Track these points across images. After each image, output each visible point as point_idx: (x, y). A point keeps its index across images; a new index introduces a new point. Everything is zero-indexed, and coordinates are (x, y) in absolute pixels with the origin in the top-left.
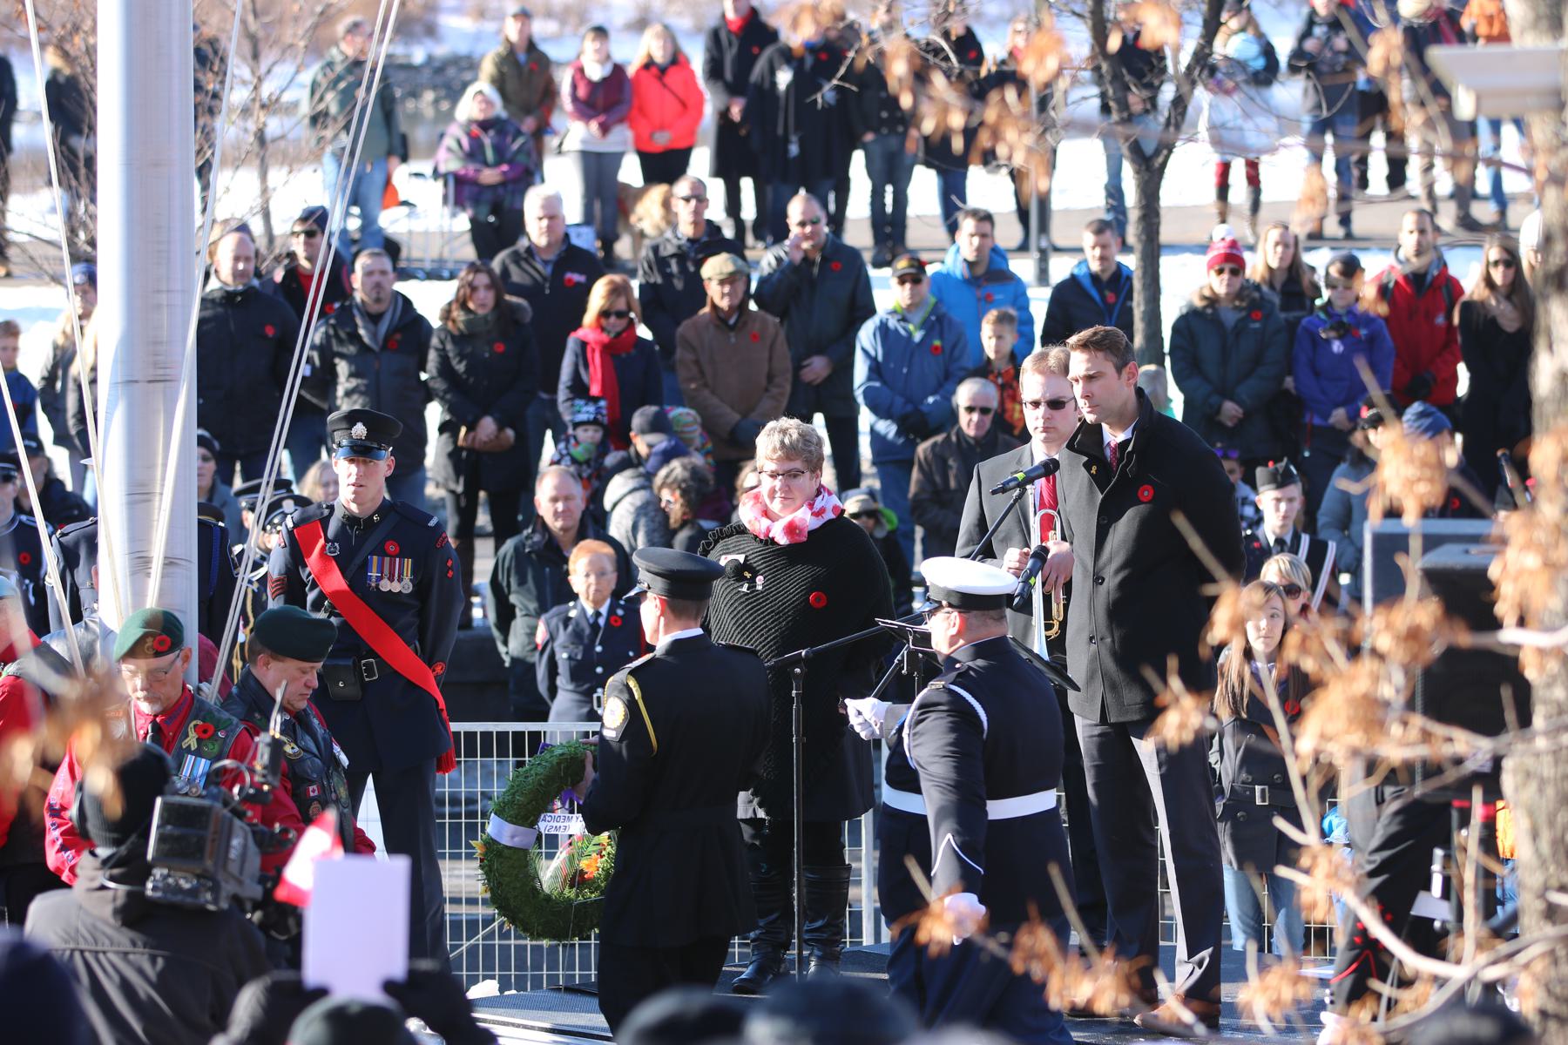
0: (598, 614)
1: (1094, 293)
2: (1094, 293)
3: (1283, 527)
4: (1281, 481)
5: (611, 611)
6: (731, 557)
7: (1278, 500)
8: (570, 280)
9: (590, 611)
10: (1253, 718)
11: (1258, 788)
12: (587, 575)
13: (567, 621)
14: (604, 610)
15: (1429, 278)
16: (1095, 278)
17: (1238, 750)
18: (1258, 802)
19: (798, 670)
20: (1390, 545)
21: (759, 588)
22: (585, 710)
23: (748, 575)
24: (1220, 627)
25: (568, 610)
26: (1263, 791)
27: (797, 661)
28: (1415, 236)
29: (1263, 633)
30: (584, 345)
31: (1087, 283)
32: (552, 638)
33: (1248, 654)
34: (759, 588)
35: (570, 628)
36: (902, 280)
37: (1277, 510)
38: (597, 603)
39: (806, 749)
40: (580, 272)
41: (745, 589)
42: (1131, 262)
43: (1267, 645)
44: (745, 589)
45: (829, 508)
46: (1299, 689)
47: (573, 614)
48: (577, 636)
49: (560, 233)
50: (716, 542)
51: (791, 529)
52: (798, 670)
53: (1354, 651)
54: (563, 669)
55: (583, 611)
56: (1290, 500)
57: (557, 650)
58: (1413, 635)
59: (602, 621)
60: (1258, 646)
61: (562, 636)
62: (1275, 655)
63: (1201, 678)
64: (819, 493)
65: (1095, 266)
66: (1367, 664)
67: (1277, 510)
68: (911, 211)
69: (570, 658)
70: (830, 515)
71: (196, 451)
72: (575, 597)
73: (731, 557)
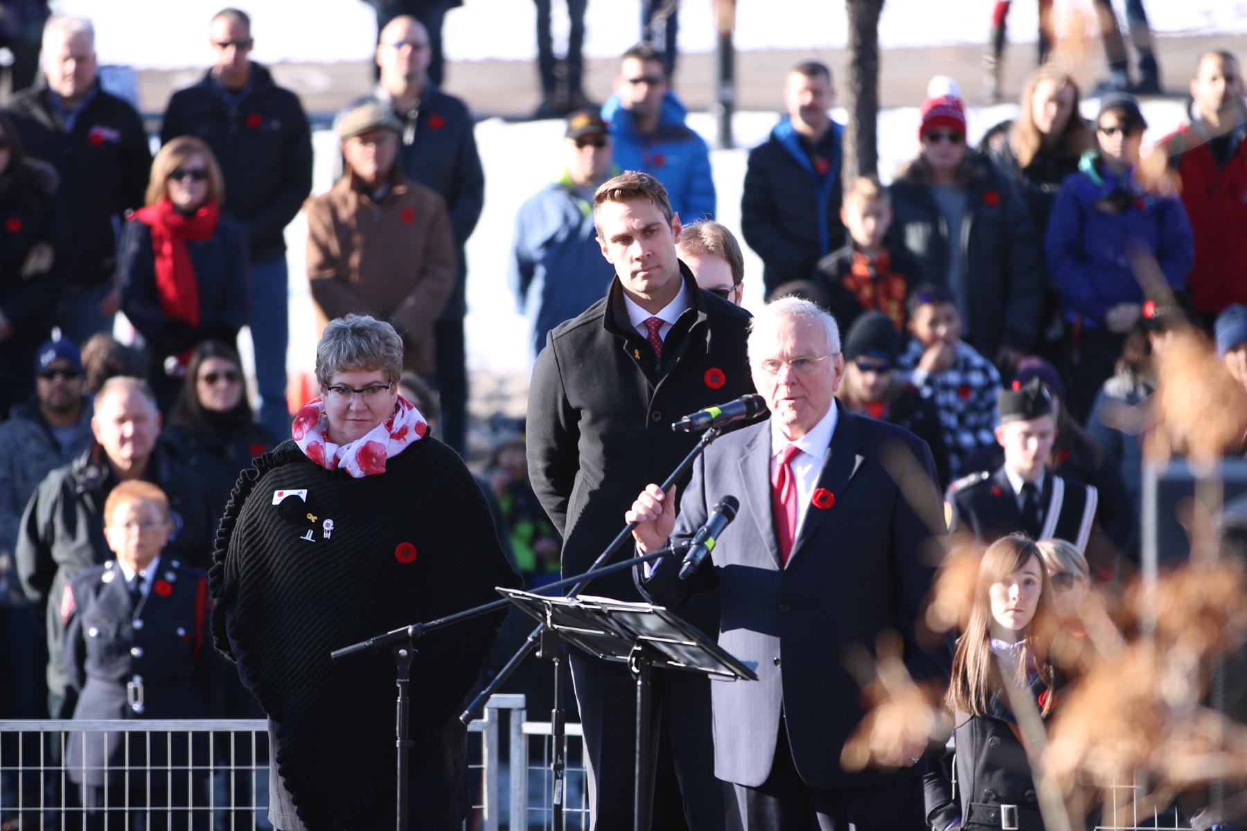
0: (139, 580)
1: (801, 157)
2: (801, 157)
3: (1033, 469)
4: (1030, 409)
5: (159, 574)
6: (287, 493)
7: (1027, 435)
8: (97, 137)
9: (130, 576)
10: (997, 721)
11: (1004, 808)
12: (128, 525)
13: (99, 587)
14: (147, 573)
15: (1234, 143)
16: (800, 139)
17: (976, 760)
18: (1005, 825)
19: (403, 652)
20: (1177, 492)
21: (327, 535)
22: (117, 704)
23: (313, 518)
24: (950, 599)
25: (103, 571)
26: (1011, 811)
27: (403, 640)
28: (1221, 85)
29: (1013, 604)
30: (147, 229)
31: (793, 147)
32: (79, 608)
33: (990, 632)
34: (327, 535)
35: (103, 596)
36: (581, 142)
37: (1025, 446)
38: (141, 563)
39: (409, 754)
40: (112, 126)
41: (309, 537)
42: (841, 115)
43: (1017, 621)
44: (309, 537)
45: (412, 425)
46: (1058, 680)
47: (108, 578)
48: (111, 605)
49: (89, 77)
50: (263, 472)
51: (365, 455)
52: (403, 652)
53: (1130, 630)
54: (93, 650)
55: (121, 575)
56: (1042, 435)
57: (85, 624)
58: (1208, 615)
59: (145, 589)
60: (1006, 620)
61: (92, 607)
62: (1024, 633)
63: (933, 662)
64: (397, 407)
65: (799, 125)
66: (1144, 652)
67: (1025, 446)
68: (592, 49)
69: (99, 635)
70: (413, 436)
71: (285, 793)
72: (113, 556)
73: (287, 493)
